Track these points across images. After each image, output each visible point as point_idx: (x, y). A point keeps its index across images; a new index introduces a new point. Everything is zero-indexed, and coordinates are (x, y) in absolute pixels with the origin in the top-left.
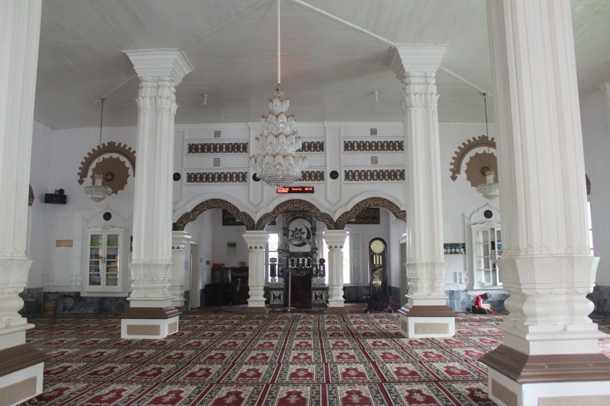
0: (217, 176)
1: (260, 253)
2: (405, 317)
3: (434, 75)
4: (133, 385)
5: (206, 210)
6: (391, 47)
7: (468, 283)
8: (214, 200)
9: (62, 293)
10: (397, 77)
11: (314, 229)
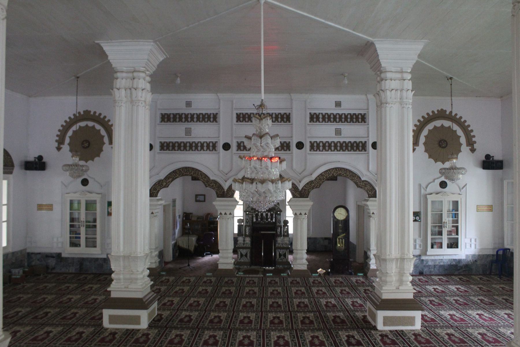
0: (188, 145)
1: (229, 219)
7: (422, 248)
8: (186, 168)
9: (44, 253)
10: (371, 68)
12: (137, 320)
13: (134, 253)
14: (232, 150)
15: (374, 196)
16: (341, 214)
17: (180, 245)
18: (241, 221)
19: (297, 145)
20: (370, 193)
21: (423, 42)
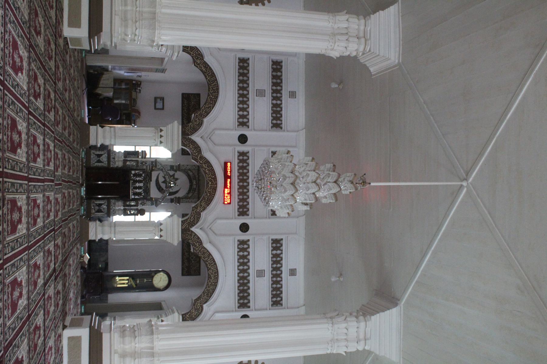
0: (245, 92)
1: (154, 141)
2: (89, 325)
3: (367, 348)
5: (206, 79)
6: (399, 300)
8: (218, 89)
10: (363, 305)
11: (178, 200)
12: (75, 23)
13: (160, 26)
14: (239, 146)
15: (184, 319)
16: (160, 280)
17: (104, 76)
18: (144, 155)
19: (245, 225)
20: (187, 316)
21: (400, 360)
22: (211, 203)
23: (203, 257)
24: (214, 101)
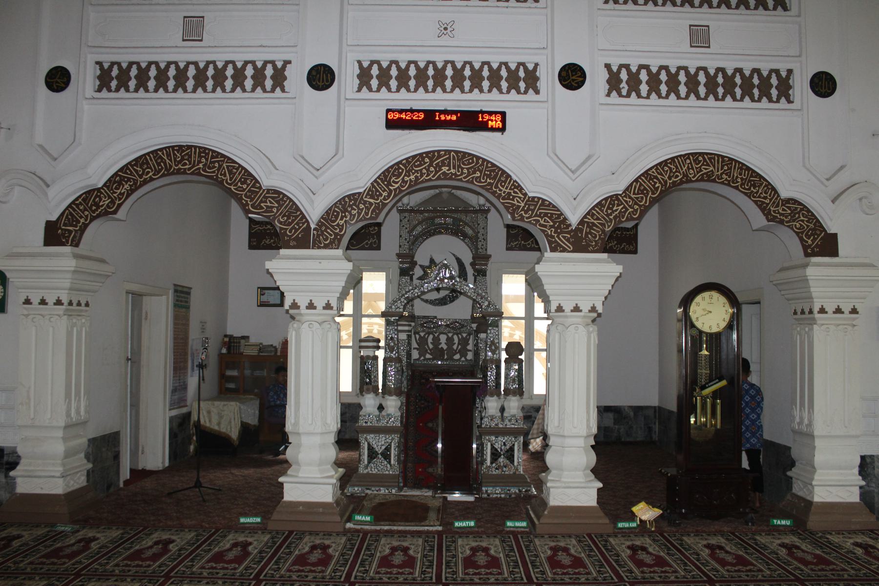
4: (183, 533)
19: (564, 74)
22: (500, 169)
23: (653, 193)
24: (213, 157)
